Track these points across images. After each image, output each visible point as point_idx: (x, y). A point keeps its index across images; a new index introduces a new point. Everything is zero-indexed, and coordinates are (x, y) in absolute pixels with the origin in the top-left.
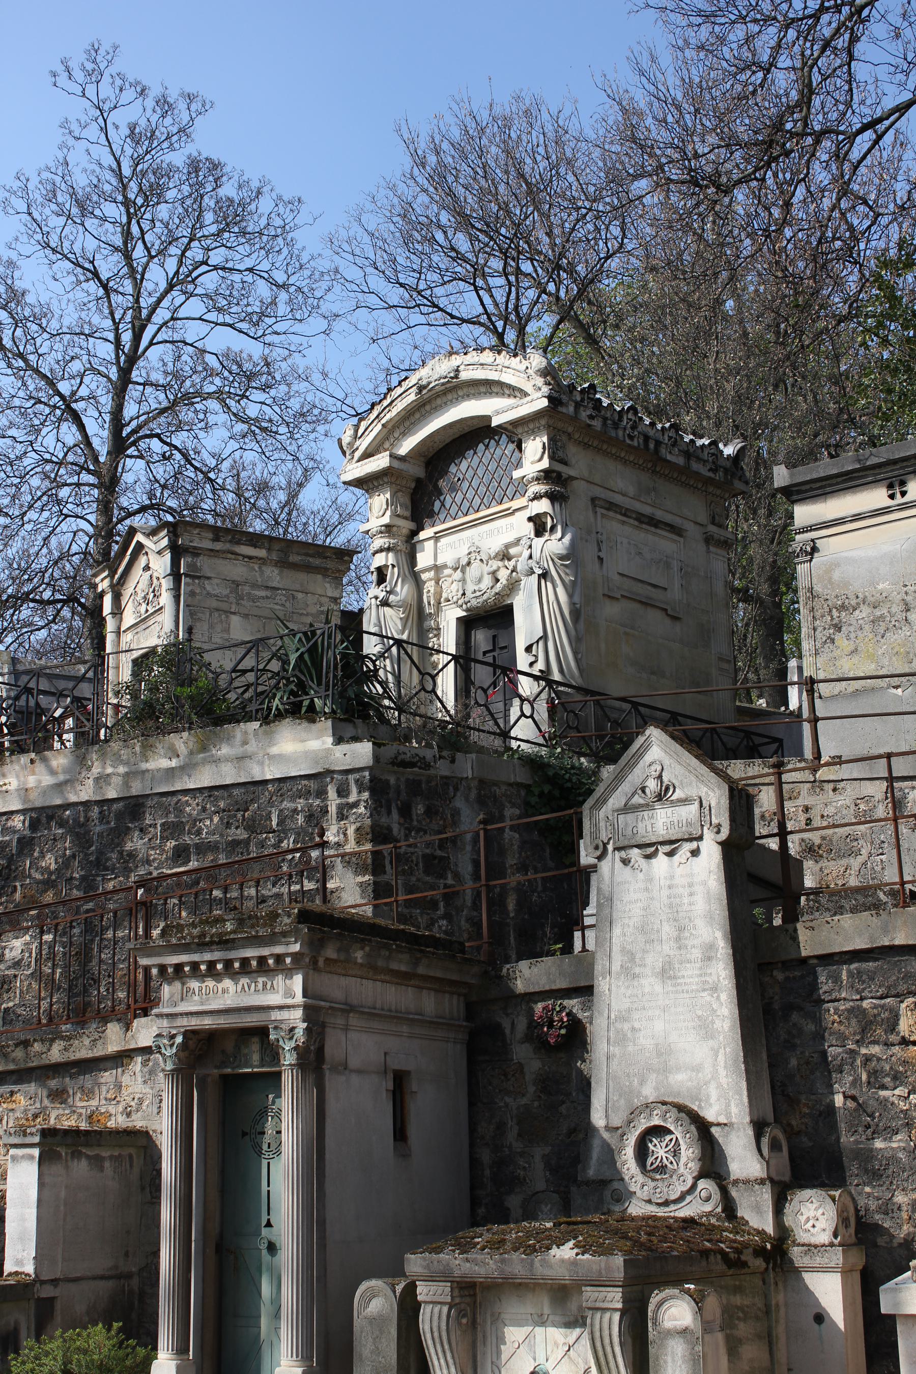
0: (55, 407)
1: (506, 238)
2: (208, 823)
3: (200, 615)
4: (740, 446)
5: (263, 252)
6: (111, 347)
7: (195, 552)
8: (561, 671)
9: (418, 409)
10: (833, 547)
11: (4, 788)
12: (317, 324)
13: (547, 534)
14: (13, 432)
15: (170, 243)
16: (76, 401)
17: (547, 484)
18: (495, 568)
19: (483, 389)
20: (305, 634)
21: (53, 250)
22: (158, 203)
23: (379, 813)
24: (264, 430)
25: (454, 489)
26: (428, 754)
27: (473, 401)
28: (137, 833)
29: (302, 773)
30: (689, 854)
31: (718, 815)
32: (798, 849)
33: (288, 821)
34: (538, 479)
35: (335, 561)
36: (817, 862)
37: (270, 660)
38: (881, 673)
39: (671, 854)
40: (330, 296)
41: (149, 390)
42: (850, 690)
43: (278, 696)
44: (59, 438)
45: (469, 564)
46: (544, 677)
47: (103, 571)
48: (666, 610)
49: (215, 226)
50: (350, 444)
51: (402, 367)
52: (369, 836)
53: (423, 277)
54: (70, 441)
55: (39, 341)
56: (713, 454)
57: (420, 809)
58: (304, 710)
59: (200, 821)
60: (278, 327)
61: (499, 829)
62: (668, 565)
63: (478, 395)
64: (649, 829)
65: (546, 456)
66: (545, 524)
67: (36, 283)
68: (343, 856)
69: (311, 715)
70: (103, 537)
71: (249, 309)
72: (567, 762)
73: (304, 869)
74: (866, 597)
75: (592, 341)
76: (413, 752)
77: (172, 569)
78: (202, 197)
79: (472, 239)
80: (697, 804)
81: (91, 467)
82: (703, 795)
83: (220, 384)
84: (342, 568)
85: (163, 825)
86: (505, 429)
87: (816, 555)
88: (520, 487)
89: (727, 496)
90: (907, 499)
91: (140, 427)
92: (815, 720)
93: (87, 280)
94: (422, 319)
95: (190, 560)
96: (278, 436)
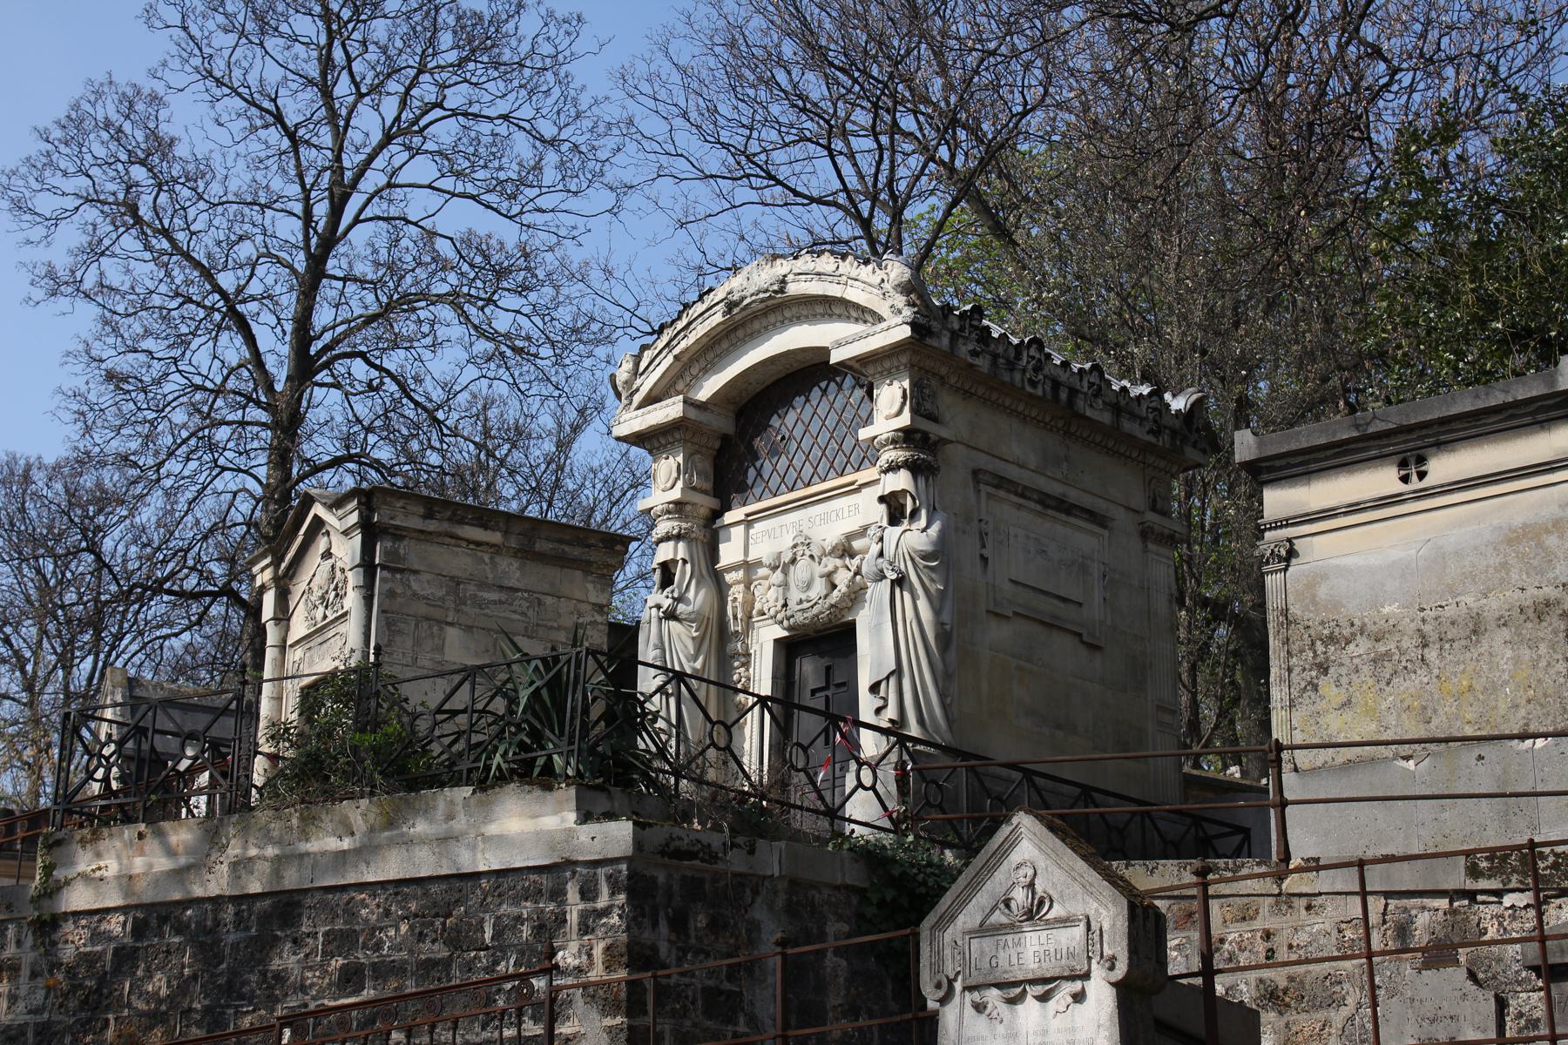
0: (213, 309)
1: (879, 81)
3: (402, 626)
4: (1195, 397)
5: (523, 92)
7: (398, 534)
9: (727, 336)
11: (98, 874)
12: (600, 198)
13: (906, 521)
14: (149, 344)
15: (389, 76)
16: (244, 301)
18: (830, 568)
19: (819, 309)
20: (544, 660)
21: (217, 80)
22: (371, 18)
23: (639, 926)
24: (518, 351)
25: (775, 452)
26: (716, 840)
27: (805, 326)
28: (288, 945)
29: (531, 863)
30: (1070, 1000)
31: (1112, 943)
32: (1254, 994)
33: (508, 934)
34: (894, 441)
35: (599, 549)
36: (1281, 1013)
37: (492, 698)
38: (1384, 737)
39: (1044, 998)
40: (619, 159)
41: (351, 288)
42: (1340, 760)
43: (501, 750)
45: (793, 561)
46: (895, 731)
47: (263, 556)
48: (1080, 635)
49: (455, 52)
52: (625, 959)
53: (755, 134)
55: (192, 213)
56: (1155, 409)
57: (701, 921)
58: (537, 771)
59: (381, 930)
60: (543, 202)
62: (1084, 570)
63: (812, 318)
64: (1014, 960)
66: (903, 506)
67: (191, 128)
68: (585, 986)
69: (546, 779)
71: (502, 175)
72: (922, 858)
73: (524, 1003)
74: (1364, 625)
75: (1001, 231)
78: (437, 9)
79: (830, 82)
80: (1082, 926)
81: (263, 399)
82: (1092, 913)
83: (455, 282)
84: (611, 561)
85: (326, 934)
86: (850, 368)
87: (1294, 561)
89: (1175, 469)
90: (1426, 483)
91: (336, 341)
92: (1284, 804)
93: (266, 127)
94: (753, 196)
95: (389, 544)
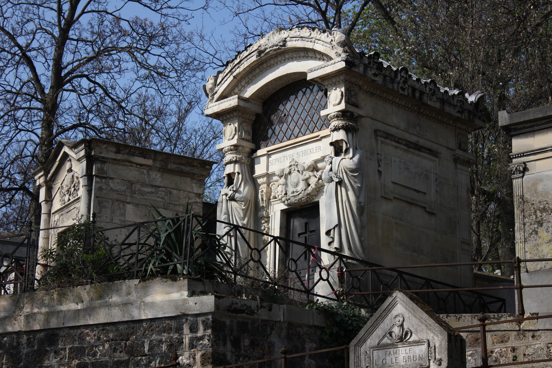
0: (15, 54)
2: (101, 348)
4: (480, 95)
6: (55, 14)
7: (103, 161)
8: (350, 248)
10: (539, 167)
13: (343, 154)
16: (30, 51)
17: (344, 120)
18: (307, 176)
19: (302, 54)
20: (172, 220)
25: (281, 122)
26: (253, 304)
27: (295, 62)
28: (52, 354)
29: (167, 315)
33: (156, 348)
34: (337, 117)
35: (198, 168)
37: (148, 237)
41: (81, 44)
42: (548, 267)
43: (153, 262)
44: (16, 77)
45: (290, 173)
47: (40, 171)
48: (425, 208)
50: (212, 89)
51: (255, 33)
52: (211, 360)
54: (25, 78)
56: (461, 101)
57: (247, 342)
58: (169, 272)
59: (96, 347)
61: (301, 357)
64: (394, 361)
65: (343, 101)
66: (342, 147)
69: (174, 276)
70: (46, 146)
72: (350, 312)
75: (388, 17)
76: (243, 303)
77: (87, 172)
80: (426, 344)
81: (39, 97)
82: (430, 339)
83: (130, 42)
84: (204, 173)
85: (70, 349)
86: (317, 82)
87: (526, 173)
88: (325, 122)
89: (470, 130)
91: (73, 70)
92: (521, 287)
95: (99, 165)
96: (170, 79)
